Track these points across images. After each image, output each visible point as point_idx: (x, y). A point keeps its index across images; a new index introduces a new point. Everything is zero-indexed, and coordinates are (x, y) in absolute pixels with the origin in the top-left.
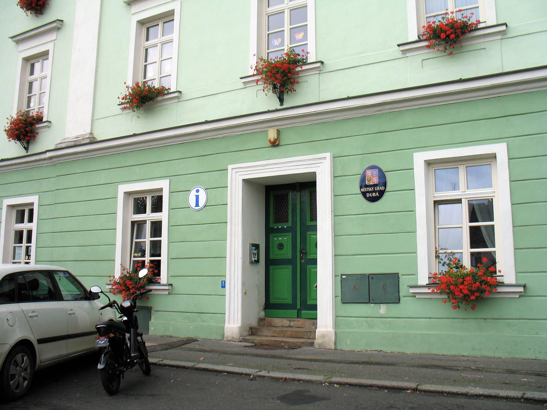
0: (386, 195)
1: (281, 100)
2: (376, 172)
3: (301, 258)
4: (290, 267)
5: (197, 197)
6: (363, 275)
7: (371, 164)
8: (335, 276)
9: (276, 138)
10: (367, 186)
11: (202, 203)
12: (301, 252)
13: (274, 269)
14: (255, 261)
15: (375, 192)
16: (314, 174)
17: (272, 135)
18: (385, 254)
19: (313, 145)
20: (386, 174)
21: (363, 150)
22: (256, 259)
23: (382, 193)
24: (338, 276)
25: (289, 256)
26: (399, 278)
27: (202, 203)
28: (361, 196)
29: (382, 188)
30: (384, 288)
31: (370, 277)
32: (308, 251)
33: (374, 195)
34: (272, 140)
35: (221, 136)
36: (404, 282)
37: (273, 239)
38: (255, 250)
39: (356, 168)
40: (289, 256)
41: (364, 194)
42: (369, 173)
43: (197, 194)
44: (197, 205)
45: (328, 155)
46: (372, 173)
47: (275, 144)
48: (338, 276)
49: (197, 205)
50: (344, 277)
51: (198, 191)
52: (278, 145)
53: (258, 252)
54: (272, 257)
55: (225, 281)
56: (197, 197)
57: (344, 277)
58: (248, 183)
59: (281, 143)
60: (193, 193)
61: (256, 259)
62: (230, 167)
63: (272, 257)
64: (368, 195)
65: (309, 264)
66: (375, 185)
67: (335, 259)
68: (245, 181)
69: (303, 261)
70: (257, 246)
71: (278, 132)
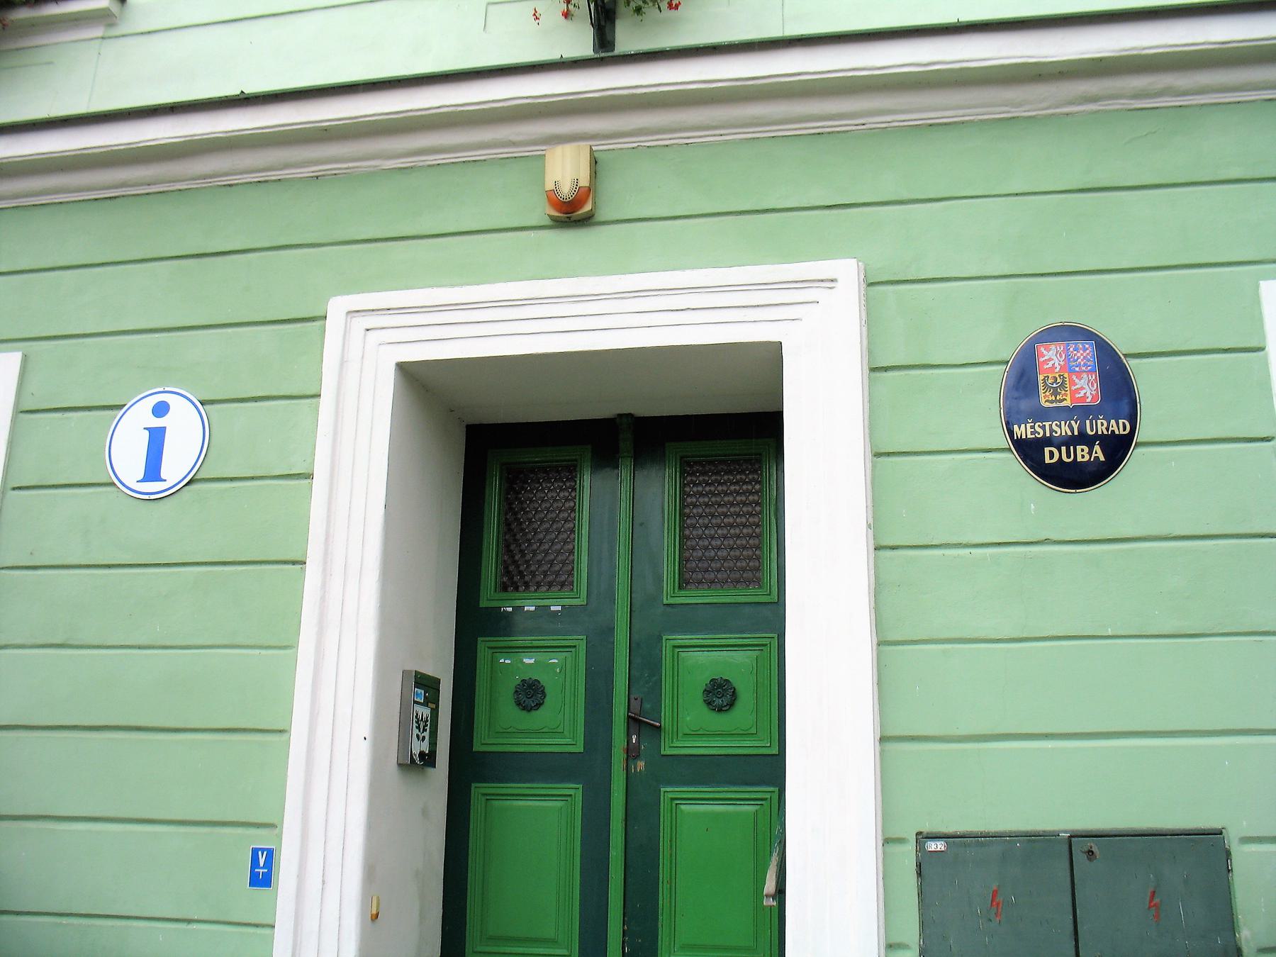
0: (1136, 457)
1: (604, 39)
2: (1084, 353)
3: (632, 753)
4: (575, 791)
5: (157, 438)
6: (1036, 841)
7: (1055, 320)
8: (887, 841)
9: (584, 182)
10: (1041, 415)
11: (175, 467)
12: (634, 722)
13: (489, 798)
14: (422, 754)
15: (1088, 441)
16: (769, 359)
17: (565, 169)
18: (1047, 736)
19: (760, 223)
20: (1132, 364)
21: (1025, 249)
22: (425, 747)
23: (1118, 448)
24: (901, 841)
25: (572, 741)
26: (1228, 854)
27: (175, 467)
28: (1013, 463)
29: (1119, 427)
30: (1154, 904)
31: (1079, 848)
32: (666, 721)
33: (1081, 453)
34: (566, 190)
35: (307, 172)
37: (493, 661)
38: (425, 704)
39: (988, 332)
40: (572, 741)
41: (1029, 451)
42: (1052, 356)
43: (157, 423)
44: (153, 471)
45: (847, 271)
46: (1068, 359)
47: (572, 213)
48: (901, 841)
49: (153, 471)
50: (933, 846)
51: (161, 409)
52: (586, 221)
53: (435, 713)
54: (483, 741)
55: (270, 854)
56: (157, 438)
57: (933, 846)
58: (418, 381)
59: (604, 213)
60: (138, 418)
61: (425, 747)
62: (337, 307)
63: (483, 741)
64: (1050, 456)
65: (670, 783)
66: (1084, 412)
67: (882, 753)
68: (404, 370)
69: (641, 764)
70: (427, 684)
71: (594, 162)
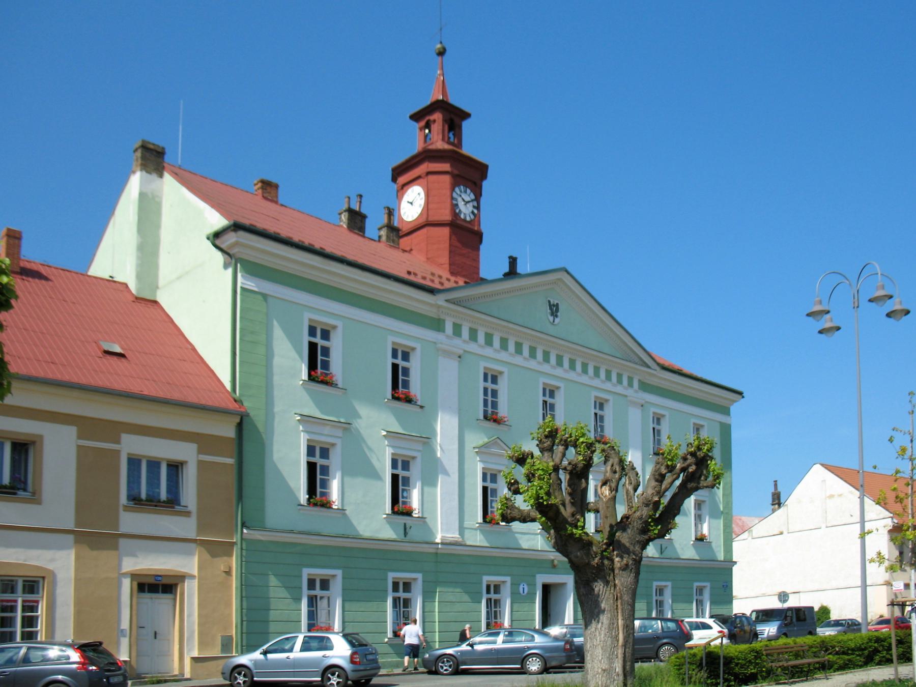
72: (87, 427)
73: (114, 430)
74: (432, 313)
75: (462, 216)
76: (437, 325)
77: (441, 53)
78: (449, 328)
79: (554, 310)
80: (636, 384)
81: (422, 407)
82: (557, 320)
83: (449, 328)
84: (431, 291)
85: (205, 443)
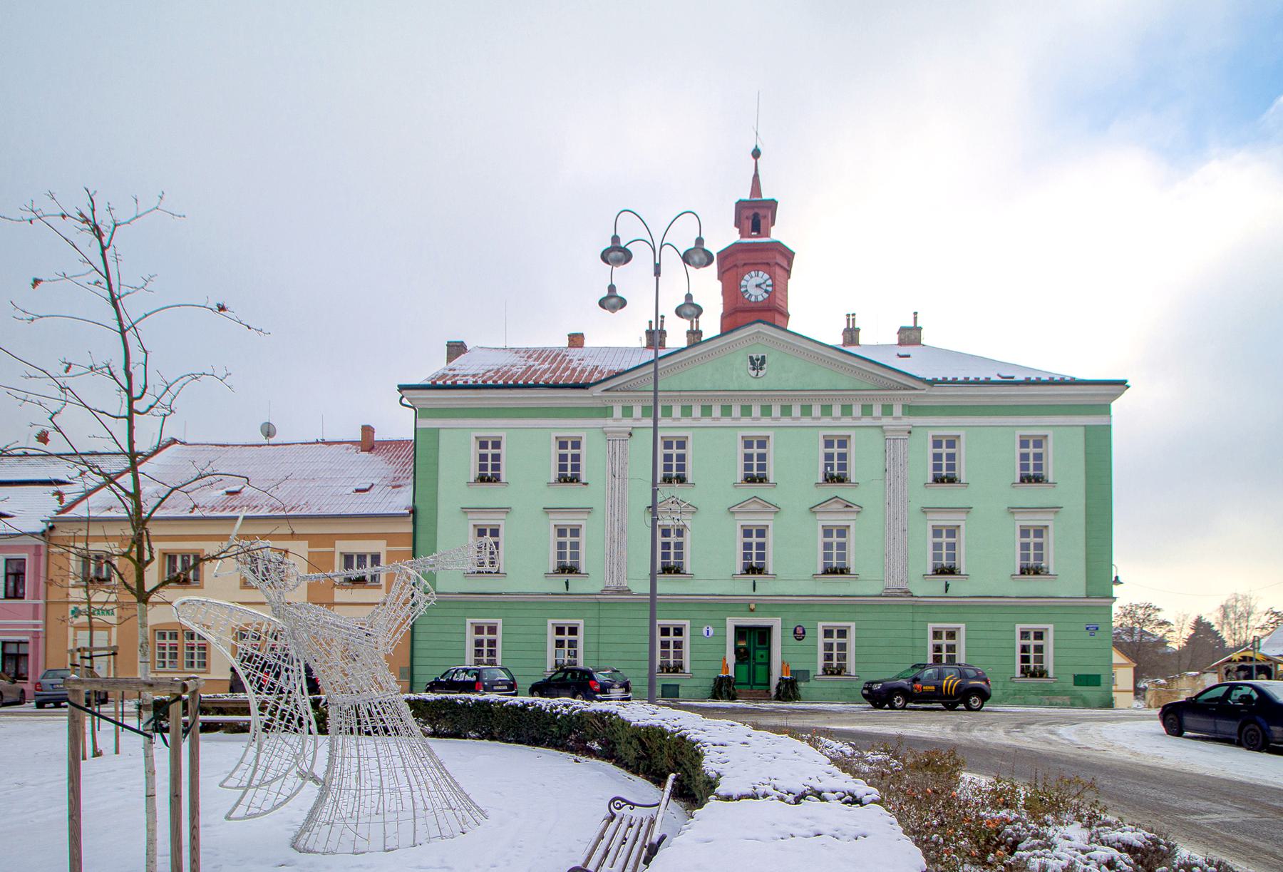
36: (811, 674)
72: (313, 539)
73: (331, 539)
74: (598, 403)
75: (753, 299)
76: (606, 412)
77: (756, 154)
78: (618, 412)
79: (757, 364)
80: (897, 410)
81: (586, 484)
82: (761, 373)
83: (618, 412)
84: (585, 386)
85: (390, 538)
